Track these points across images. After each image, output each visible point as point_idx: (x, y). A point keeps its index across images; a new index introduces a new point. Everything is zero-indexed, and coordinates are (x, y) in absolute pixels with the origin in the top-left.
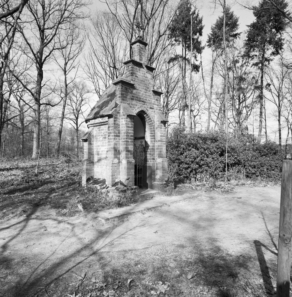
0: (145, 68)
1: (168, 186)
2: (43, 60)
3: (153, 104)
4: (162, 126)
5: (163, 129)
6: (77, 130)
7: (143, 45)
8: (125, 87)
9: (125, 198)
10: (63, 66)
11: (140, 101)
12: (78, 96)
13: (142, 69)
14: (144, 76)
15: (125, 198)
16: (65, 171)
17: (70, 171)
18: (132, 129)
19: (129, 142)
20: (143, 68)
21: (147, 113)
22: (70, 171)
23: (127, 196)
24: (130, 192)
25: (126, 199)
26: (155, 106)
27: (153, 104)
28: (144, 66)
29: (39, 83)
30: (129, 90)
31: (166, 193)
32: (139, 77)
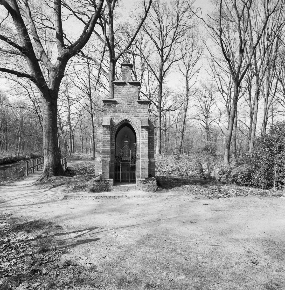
0: (129, 85)
1: (147, 183)
2: (163, 75)
3: (138, 112)
4: (143, 131)
5: (144, 134)
6: (207, 128)
7: (126, 67)
8: (108, 104)
9: (98, 187)
10: (185, 74)
11: (123, 112)
12: (207, 96)
13: (126, 86)
14: (128, 92)
15: (98, 187)
16: (169, 166)
17: (173, 167)
18: (109, 135)
19: (105, 146)
20: (127, 85)
21: (131, 121)
22: (173, 167)
23: (100, 185)
24: (103, 182)
25: (99, 187)
26: (140, 114)
27: (138, 112)
28: (128, 83)
29: (160, 94)
30: (112, 106)
31: (144, 189)
32: (122, 93)
